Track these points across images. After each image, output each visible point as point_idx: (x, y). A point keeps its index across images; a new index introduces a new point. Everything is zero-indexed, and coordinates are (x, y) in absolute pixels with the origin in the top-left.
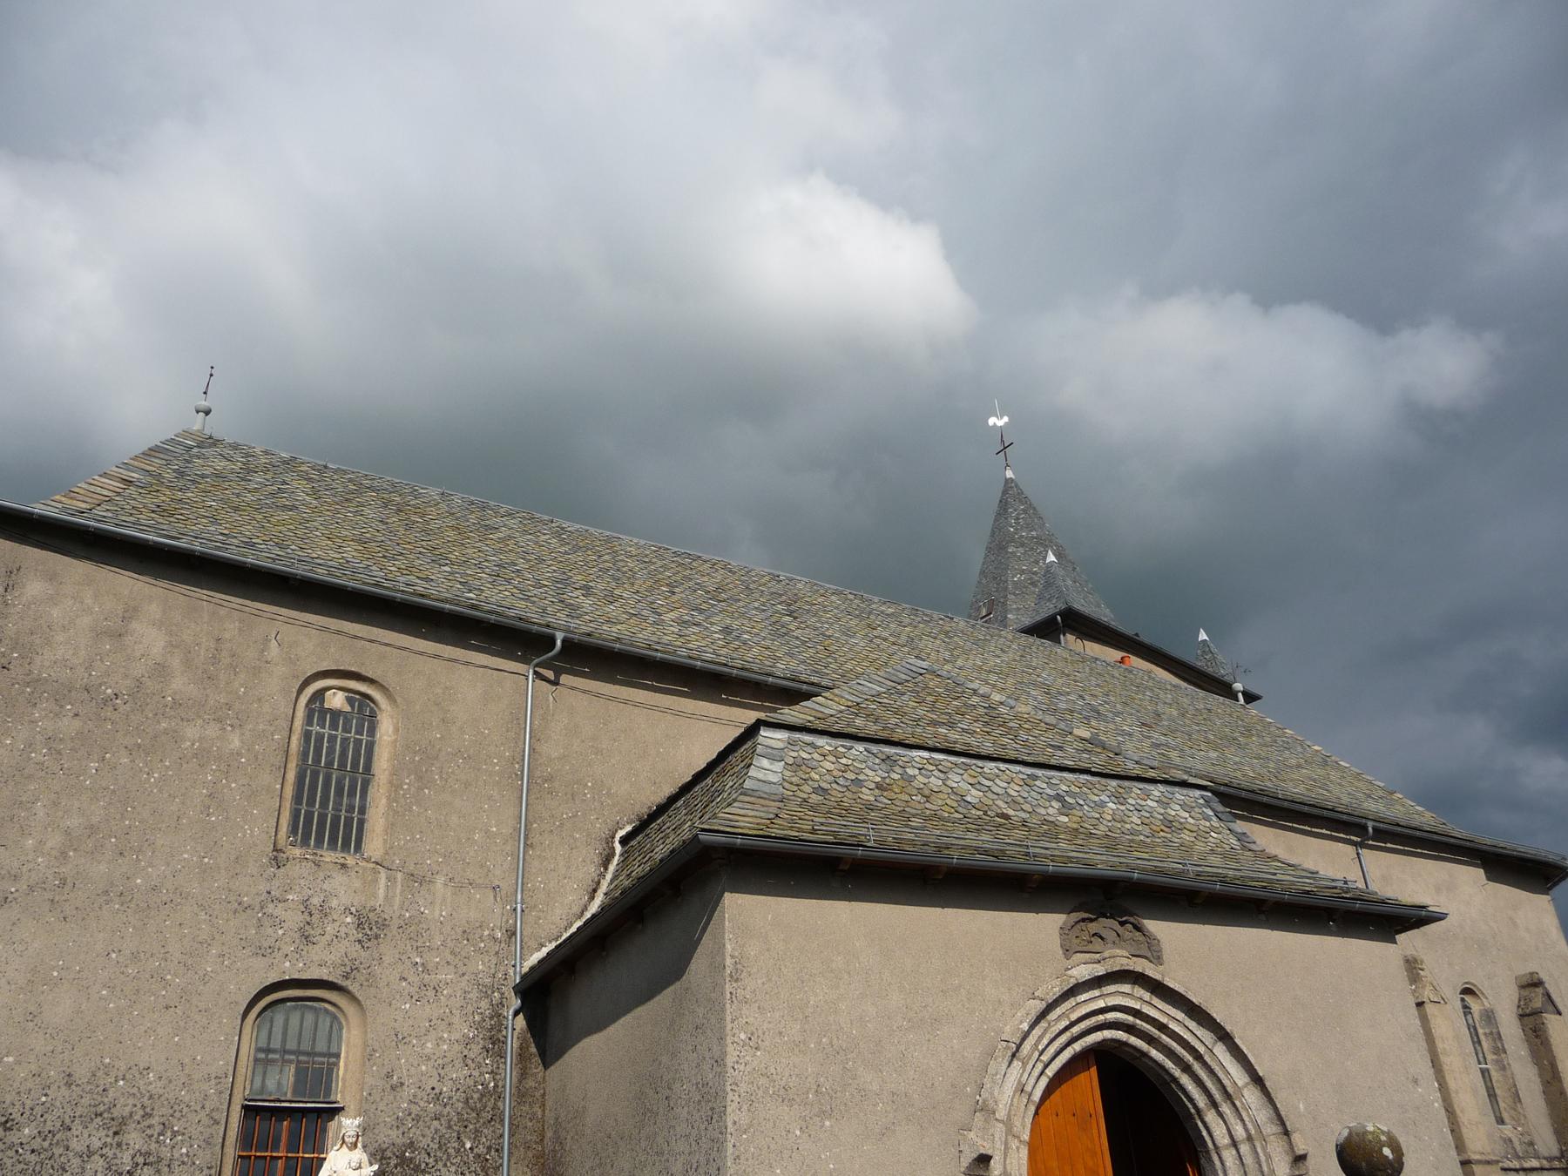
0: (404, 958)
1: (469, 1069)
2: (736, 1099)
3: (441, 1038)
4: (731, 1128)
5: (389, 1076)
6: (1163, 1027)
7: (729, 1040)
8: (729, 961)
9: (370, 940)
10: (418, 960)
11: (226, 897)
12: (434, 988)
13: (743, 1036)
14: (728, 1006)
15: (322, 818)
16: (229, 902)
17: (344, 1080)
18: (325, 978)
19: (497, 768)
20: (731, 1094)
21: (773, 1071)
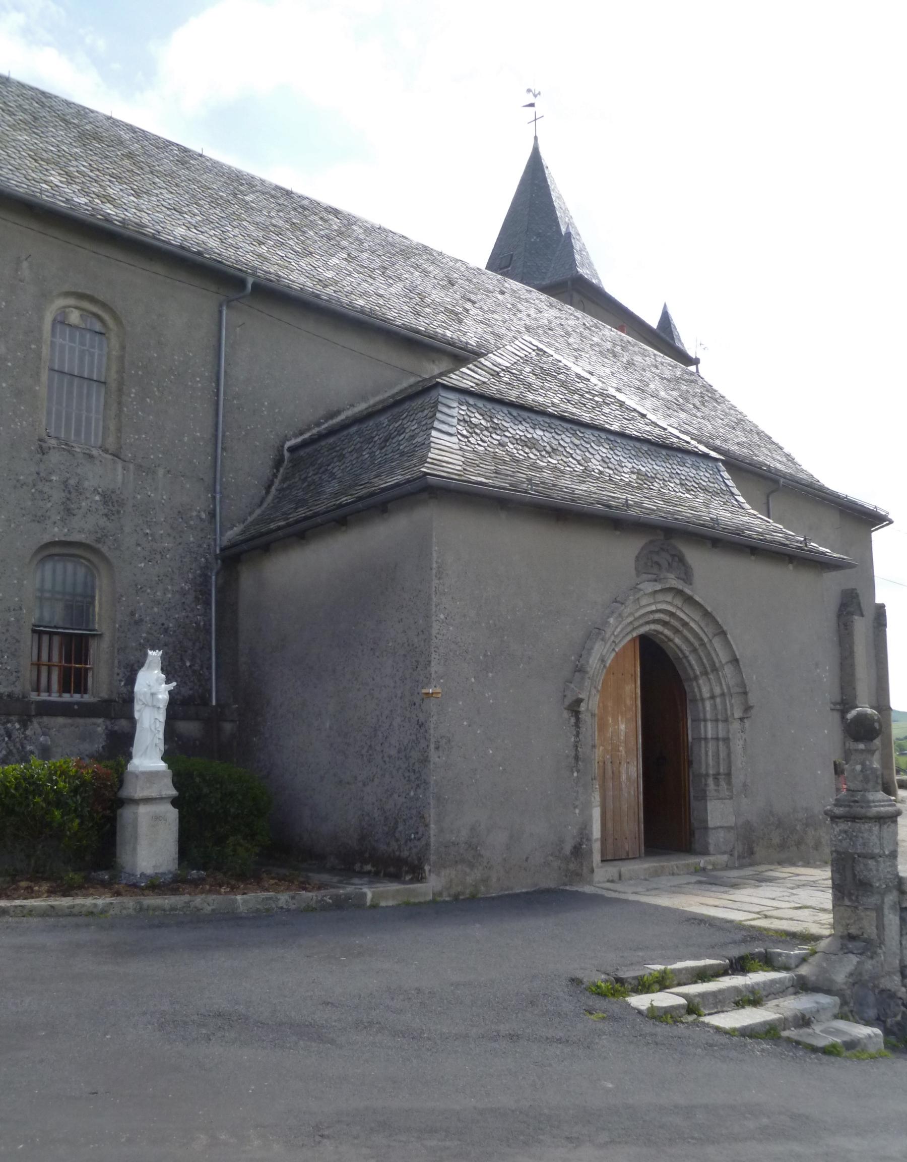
0: (138, 529)
1: (186, 612)
2: (437, 657)
3: (167, 589)
4: (433, 676)
5: (132, 614)
6: (685, 624)
7: (434, 618)
8: (434, 565)
9: (113, 514)
10: (148, 531)
11: (8, 475)
12: (161, 553)
13: (442, 616)
14: (433, 596)
15: (68, 419)
16: (10, 479)
17: (100, 615)
18: (84, 541)
19: (200, 385)
20: (434, 653)
21: (459, 640)
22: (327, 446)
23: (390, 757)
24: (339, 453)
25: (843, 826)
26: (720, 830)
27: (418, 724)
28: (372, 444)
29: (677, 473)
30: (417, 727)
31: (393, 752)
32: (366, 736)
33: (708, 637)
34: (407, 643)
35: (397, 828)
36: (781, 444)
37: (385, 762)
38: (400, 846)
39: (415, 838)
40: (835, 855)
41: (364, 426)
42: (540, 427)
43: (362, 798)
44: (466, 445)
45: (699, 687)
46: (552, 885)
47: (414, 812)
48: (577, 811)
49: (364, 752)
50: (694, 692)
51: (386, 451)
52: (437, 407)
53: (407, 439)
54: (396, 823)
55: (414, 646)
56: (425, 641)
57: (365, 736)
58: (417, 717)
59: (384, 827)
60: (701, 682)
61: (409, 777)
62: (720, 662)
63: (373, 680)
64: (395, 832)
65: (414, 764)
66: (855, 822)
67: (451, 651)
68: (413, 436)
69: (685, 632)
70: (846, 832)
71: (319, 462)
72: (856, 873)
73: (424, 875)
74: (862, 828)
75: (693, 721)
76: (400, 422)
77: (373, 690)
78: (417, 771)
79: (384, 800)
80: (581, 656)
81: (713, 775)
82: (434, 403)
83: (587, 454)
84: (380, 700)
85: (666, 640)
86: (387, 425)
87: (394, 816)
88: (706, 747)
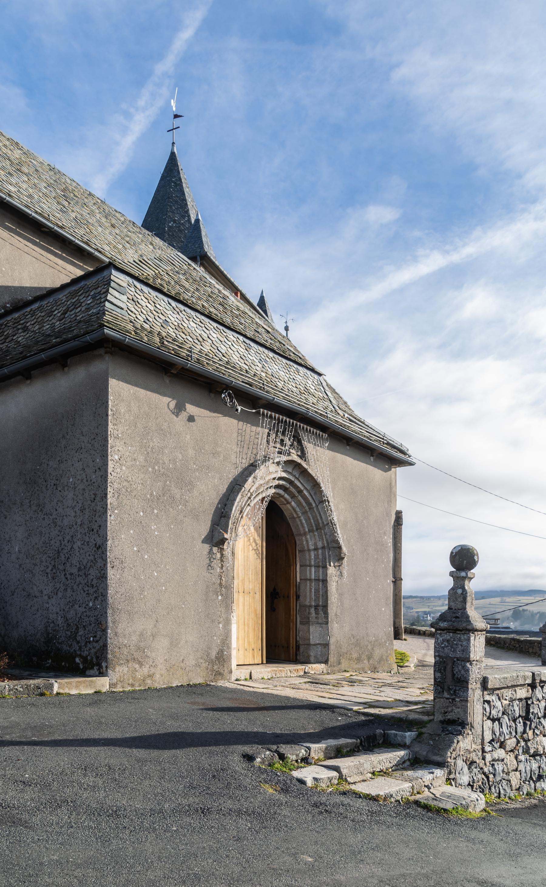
6: (300, 492)
21: (130, 479)
22: (12, 321)
23: (71, 574)
24: (23, 326)
25: (448, 636)
26: (318, 646)
27: (95, 547)
28: (53, 316)
29: (293, 379)
30: (96, 549)
31: (74, 570)
32: (50, 558)
33: (316, 504)
34: (85, 479)
35: (77, 633)
36: (341, 395)
37: (67, 578)
38: (80, 648)
39: (93, 640)
40: (438, 659)
41: (44, 303)
42: (194, 320)
43: (48, 609)
44: (134, 320)
45: (307, 541)
46: (199, 680)
47: (93, 619)
48: (221, 626)
49: (48, 570)
50: (302, 544)
51: (65, 321)
52: (110, 284)
53: (83, 311)
54: (77, 628)
55: (92, 482)
56: (101, 477)
57: (49, 557)
58: (95, 541)
59: (66, 632)
60: (308, 537)
61: (88, 591)
62: (323, 523)
63: (56, 510)
64: (76, 636)
65: (92, 580)
66: (455, 633)
67: (123, 487)
68: (88, 308)
69: (300, 498)
70: (448, 641)
71: (6, 333)
72: (455, 672)
73: (101, 670)
74: (462, 638)
75: (301, 566)
76: (77, 298)
77: (56, 519)
78: (95, 586)
79: (66, 610)
80: (225, 505)
81: (315, 606)
82: (107, 281)
83: (229, 349)
84: (62, 528)
85: (285, 503)
86: (65, 301)
87: (75, 623)
88: (310, 585)
